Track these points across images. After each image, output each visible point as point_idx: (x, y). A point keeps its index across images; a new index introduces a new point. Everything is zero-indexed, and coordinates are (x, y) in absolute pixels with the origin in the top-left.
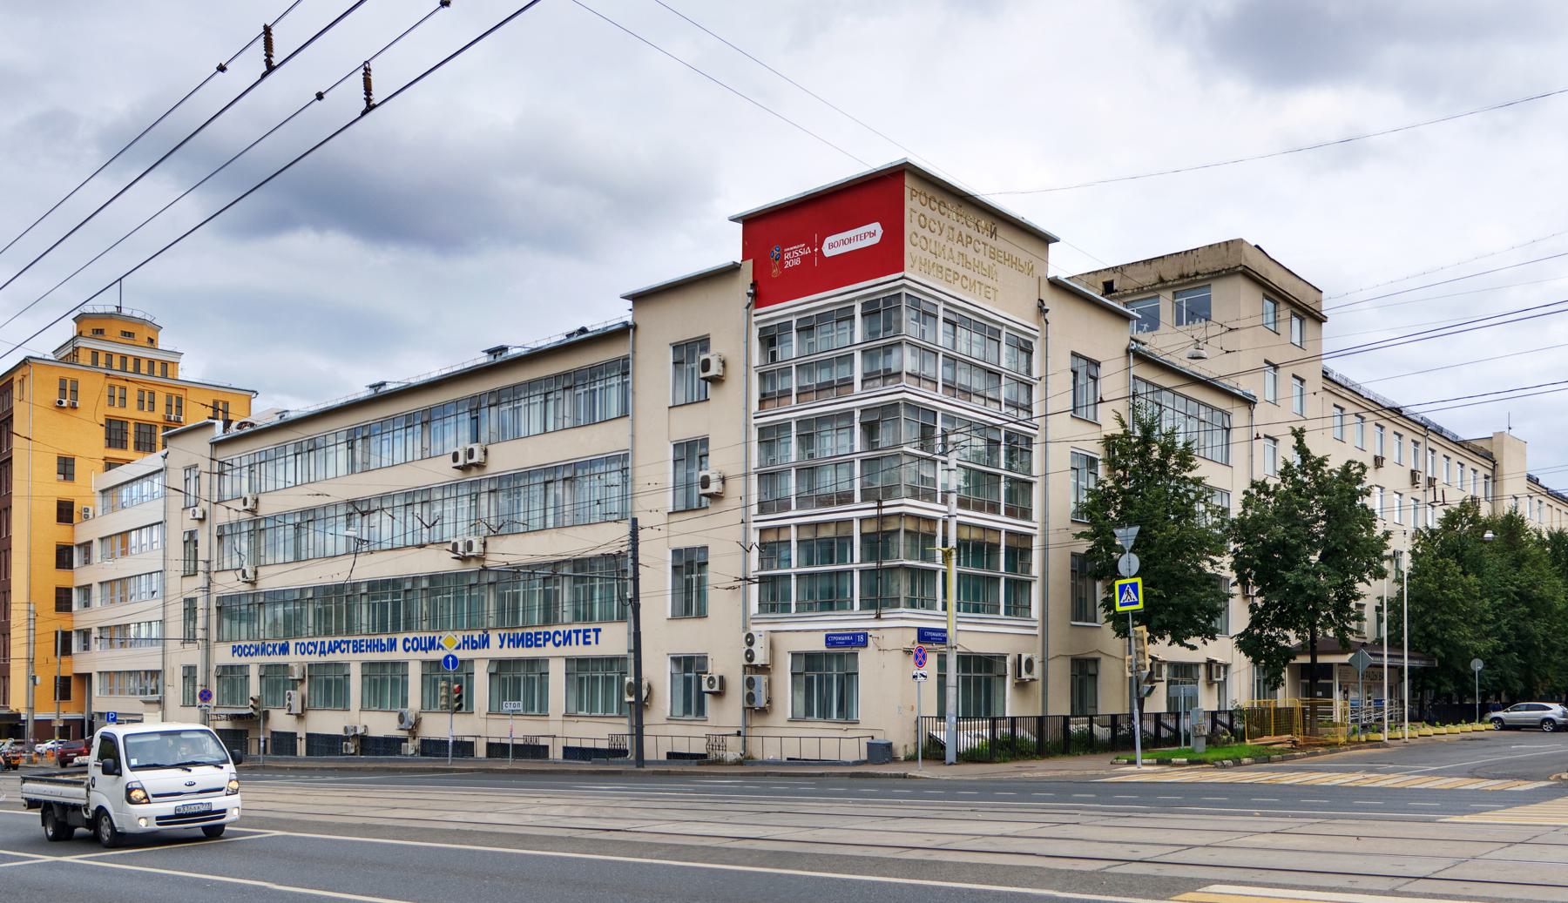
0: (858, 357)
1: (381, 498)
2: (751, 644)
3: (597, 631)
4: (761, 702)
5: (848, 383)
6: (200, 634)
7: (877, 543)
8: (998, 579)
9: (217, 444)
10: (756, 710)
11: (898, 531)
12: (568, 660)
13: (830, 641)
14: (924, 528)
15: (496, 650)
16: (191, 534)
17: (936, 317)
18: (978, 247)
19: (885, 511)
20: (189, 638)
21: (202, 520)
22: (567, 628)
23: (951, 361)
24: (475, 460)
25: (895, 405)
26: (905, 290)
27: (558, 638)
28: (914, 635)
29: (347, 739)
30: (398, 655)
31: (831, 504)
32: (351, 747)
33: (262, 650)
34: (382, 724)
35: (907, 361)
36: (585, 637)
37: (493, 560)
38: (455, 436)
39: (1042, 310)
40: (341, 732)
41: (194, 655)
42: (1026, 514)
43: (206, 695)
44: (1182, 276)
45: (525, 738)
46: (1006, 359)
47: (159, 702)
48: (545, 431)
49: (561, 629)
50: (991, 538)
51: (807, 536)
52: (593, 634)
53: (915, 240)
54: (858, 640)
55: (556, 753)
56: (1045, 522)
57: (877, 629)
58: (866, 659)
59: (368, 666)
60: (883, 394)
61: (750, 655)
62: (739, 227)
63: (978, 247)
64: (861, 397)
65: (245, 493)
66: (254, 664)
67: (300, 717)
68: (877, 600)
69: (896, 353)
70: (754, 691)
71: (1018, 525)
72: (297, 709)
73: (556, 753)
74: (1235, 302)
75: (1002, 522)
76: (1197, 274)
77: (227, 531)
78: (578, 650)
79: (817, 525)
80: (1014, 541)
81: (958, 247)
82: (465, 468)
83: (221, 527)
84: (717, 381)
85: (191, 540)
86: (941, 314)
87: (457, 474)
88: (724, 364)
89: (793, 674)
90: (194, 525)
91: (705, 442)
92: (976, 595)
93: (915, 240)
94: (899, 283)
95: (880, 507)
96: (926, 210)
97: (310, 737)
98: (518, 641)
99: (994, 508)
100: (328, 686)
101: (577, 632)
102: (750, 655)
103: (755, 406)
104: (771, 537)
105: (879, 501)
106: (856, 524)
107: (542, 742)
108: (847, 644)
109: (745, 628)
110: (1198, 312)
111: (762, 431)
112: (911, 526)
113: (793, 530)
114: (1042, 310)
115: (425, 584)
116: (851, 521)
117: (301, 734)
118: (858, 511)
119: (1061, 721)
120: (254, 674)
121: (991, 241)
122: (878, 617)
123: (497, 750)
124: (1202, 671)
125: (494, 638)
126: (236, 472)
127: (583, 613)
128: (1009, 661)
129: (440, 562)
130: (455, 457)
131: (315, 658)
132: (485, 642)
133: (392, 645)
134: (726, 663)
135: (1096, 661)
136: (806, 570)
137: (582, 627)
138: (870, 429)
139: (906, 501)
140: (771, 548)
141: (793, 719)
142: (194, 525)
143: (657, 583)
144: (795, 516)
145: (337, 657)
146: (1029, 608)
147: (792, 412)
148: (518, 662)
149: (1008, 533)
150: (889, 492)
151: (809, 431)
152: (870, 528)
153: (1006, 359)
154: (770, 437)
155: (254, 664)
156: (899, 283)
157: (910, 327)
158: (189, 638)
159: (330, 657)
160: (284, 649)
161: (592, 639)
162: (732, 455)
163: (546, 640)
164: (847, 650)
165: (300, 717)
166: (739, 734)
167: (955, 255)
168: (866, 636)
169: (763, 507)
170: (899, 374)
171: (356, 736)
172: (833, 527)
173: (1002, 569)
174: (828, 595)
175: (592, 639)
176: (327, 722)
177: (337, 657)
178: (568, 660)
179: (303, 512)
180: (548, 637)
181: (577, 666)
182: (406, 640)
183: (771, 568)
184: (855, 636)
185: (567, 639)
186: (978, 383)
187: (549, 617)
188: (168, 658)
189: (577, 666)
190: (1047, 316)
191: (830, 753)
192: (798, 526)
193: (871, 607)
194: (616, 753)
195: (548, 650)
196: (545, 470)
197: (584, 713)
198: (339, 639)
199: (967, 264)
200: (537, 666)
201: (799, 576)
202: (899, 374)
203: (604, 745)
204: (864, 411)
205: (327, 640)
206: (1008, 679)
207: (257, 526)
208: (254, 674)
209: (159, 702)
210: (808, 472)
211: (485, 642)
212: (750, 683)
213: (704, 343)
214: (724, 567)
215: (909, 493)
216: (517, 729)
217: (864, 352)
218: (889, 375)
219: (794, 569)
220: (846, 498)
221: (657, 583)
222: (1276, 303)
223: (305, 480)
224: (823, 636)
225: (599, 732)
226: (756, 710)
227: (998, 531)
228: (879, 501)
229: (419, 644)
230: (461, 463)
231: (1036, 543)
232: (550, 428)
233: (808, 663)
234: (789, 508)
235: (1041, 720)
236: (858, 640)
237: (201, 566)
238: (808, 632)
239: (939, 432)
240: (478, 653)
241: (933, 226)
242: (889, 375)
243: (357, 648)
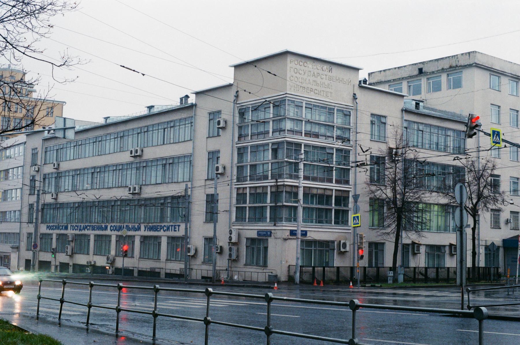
0: (271, 123)
1: (105, 167)
2: (231, 234)
3: (179, 226)
4: (234, 257)
5: (268, 132)
6: (34, 221)
7: (276, 194)
8: (331, 210)
9: (45, 140)
10: (234, 261)
11: (283, 191)
12: (168, 237)
13: (259, 234)
14: (294, 190)
15: (143, 232)
16: (33, 177)
17: (302, 107)
18: (322, 76)
19: (279, 184)
20: (30, 222)
21: (38, 171)
22: (169, 224)
23: (308, 122)
24: (138, 154)
25: (283, 142)
26: (287, 98)
27: (165, 228)
28: (288, 233)
29: (87, 266)
30: (108, 232)
31: (261, 180)
32: (89, 270)
33: (58, 228)
34: (101, 261)
35: (289, 125)
36: (175, 228)
37: (144, 195)
38: (132, 143)
39: (355, 97)
40: (85, 263)
41: (31, 229)
42: (347, 182)
43: (35, 246)
44: (451, 67)
45: (151, 268)
46: (338, 120)
47: (17, 248)
48: (164, 144)
49: (166, 224)
50: (328, 193)
51: (253, 192)
52: (177, 227)
53: (292, 78)
54: (268, 234)
55: (163, 276)
56: (355, 185)
57: (275, 230)
58: (271, 242)
59: (97, 236)
60: (279, 138)
61: (230, 238)
62: (233, 68)
63: (322, 76)
64: (271, 139)
65: (55, 162)
66: (55, 233)
67: (71, 256)
68: (275, 219)
69: (283, 123)
70: (232, 253)
71: (343, 187)
72: (69, 253)
73: (163, 276)
74: (475, 79)
75: (334, 186)
76: (457, 66)
77: (47, 176)
78: (171, 233)
79: (256, 187)
80: (340, 194)
81: (313, 78)
82: (135, 157)
83: (45, 175)
84: (223, 128)
85: (33, 180)
86: (304, 105)
87: (132, 159)
88: (226, 122)
89: (247, 246)
90: (34, 173)
91: (218, 152)
92: (321, 217)
93: (292, 78)
94: (285, 96)
95: (277, 182)
96: (298, 67)
97: (74, 265)
98: (151, 229)
99: (330, 181)
100: (80, 243)
101: (172, 226)
102: (230, 238)
103: (236, 139)
104: (241, 191)
105: (277, 180)
106: (269, 189)
107: (157, 270)
108: (264, 235)
109: (230, 227)
110: (457, 84)
111: (239, 149)
112: (288, 189)
113: (248, 189)
114: (355, 97)
115: (119, 203)
116: (267, 187)
117: (71, 264)
118: (269, 183)
119: (349, 270)
120: (54, 237)
121: (330, 74)
122: (275, 225)
123: (141, 273)
124: (447, 249)
125: (143, 228)
126: (52, 152)
127: (173, 218)
128: (336, 243)
129: (123, 194)
130: (131, 153)
131: (77, 232)
132: (139, 229)
133: (106, 228)
134: (222, 241)
135: (383, 244)
136: (250, 206)
137: (174, 224)
138: (275, 151)
139: (285, 180)
140: (241, 196)
141: (246, 265)
142: (34, 173)
143: (199, 208)
144: (248, 184)
145: (86, 232)
146: (348, 221)
147: (249, 142)
148: (151, 237)
149: (336, 190)
150: (280, 176)
151: (256, 149)
152: (274, 190)
153: (338, 120)
154: (241, 152)
155: (55, 233)
156: (285, 96)
157: (291, 112)
158: (30, 222)
159: (83, 232)
160: (66, 228)
161: (177, 229)
162: (227, 159)
163: (161, 229)
164: (264, 238)
165: (71, 256)
166: (226, 270)
167: (311, 81)
168: (271, 233)
169: (238, 180)
170: (284, 130)
171: (91, 265)
172: (261, 188)
173: (333, 205)
174: (258, 215)
175: (177, 229)
176: (81, 259)
177: (86, 232)
178: (168, 237)
179: (76, 170)
180: (162, 228)
181: (172, 240)
182: (111, 226)
183: (240, 204)
184: (267, 232)
185: (168, 229)
186: (322, 131)
187: (162, 219)
188: (22, 230)
189: (172, 240)
190: (357, 101)
191: (255, 277)
192: (250, 188)
193: (273, 221)
194: (180, 276)
195: (161, 233)
196: (162, 159)
197: (174, 259)
198: (87, 225)
199: (317, 84)
200: (157, 238)
201: (250, 207)
202: (284, 130)
203: (178, 272)
204: (273, 144)
205: (82, 225)
206: (335, 251)
207: (59, 175)
208: (54, 237)
209: (17, 248)
210: (253, 167)
211: (139, 229)
212: (230, 249)
213: (219, 112)
214: (223, 204)
215: (288, 176)
216: (147, 265)
217: (273, 121)
218: (281, 130)
219: (248, 205)
220: (266, 178)
221: (199, 208)
222: (499, 77)
223: (77, 157)
224: (256, 232)
225: (176, 267)
226: (234, 261)
227: (332, 190)
228: (277, 180)
229: (116, 228)
230: (133, 155)
231: (351, 194)
232: (165, 143)
233: (252, 241)
234: (247, 181)
235: (352, 269)
236: (268, 234)
237: (36, 192)
238: (251, 231)
239: (303, 152)
240: (137, 233)
241: (300, 72)
242: (281, 130)
243: (93, 229)
